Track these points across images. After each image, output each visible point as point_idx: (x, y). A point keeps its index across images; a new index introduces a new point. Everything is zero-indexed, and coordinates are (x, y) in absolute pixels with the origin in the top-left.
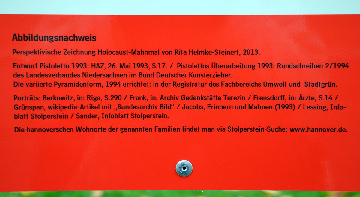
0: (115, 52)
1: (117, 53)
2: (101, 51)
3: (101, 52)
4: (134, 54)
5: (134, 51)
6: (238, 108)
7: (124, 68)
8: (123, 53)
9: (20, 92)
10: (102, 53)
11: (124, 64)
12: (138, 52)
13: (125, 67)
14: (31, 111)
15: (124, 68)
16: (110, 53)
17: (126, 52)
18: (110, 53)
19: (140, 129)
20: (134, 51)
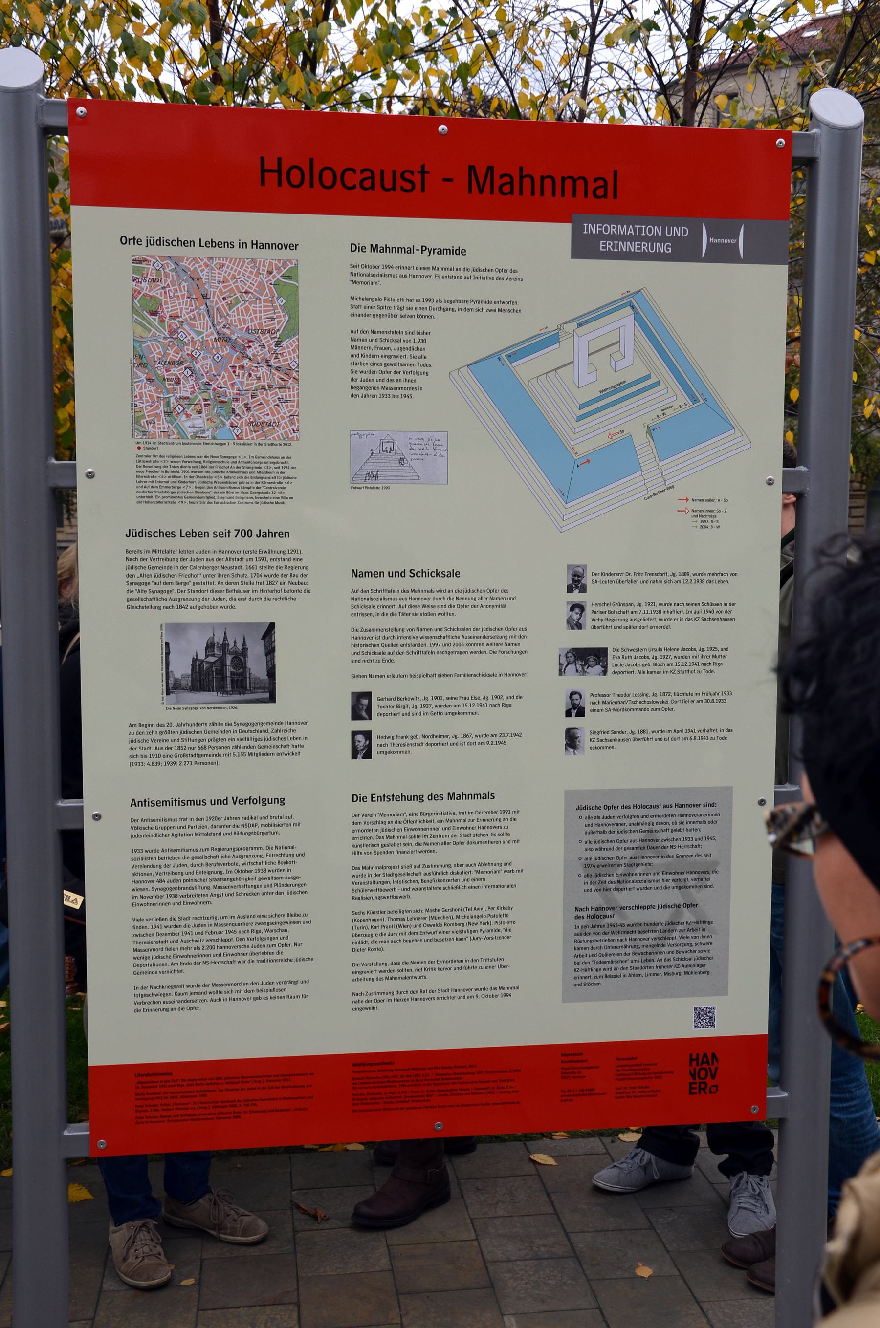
0: (354, 171)
1: (368, 184)
2: (267, 175)
3: (279, 171)
4: (481, 191)
5: (481, 173)
6: (656, 889)
7: (492, 192)
8: (400, 182)
9: (141, 452)
10: (284, 177)
11: (490, 169)
12: (502, 176)
13: (496, 189)
14: (137, 587)
15: (492, 192)
16: (328, 178)
17: (417, 179)
18: (328, 178)
19: (165, 803)
20: (481, 173)
